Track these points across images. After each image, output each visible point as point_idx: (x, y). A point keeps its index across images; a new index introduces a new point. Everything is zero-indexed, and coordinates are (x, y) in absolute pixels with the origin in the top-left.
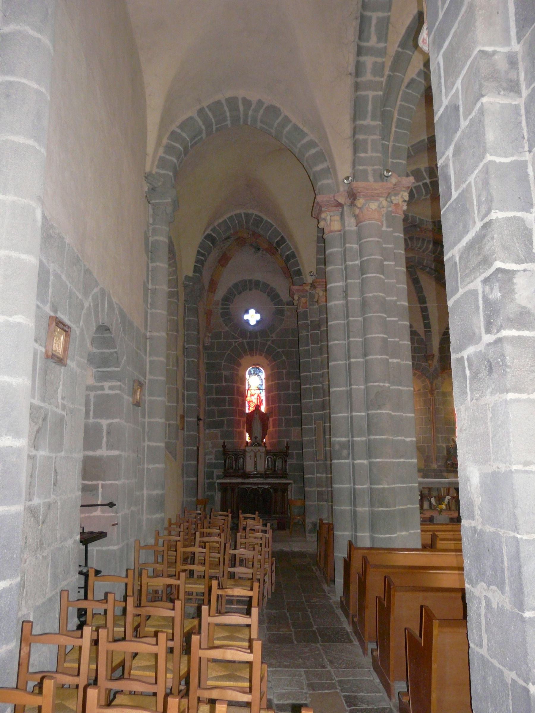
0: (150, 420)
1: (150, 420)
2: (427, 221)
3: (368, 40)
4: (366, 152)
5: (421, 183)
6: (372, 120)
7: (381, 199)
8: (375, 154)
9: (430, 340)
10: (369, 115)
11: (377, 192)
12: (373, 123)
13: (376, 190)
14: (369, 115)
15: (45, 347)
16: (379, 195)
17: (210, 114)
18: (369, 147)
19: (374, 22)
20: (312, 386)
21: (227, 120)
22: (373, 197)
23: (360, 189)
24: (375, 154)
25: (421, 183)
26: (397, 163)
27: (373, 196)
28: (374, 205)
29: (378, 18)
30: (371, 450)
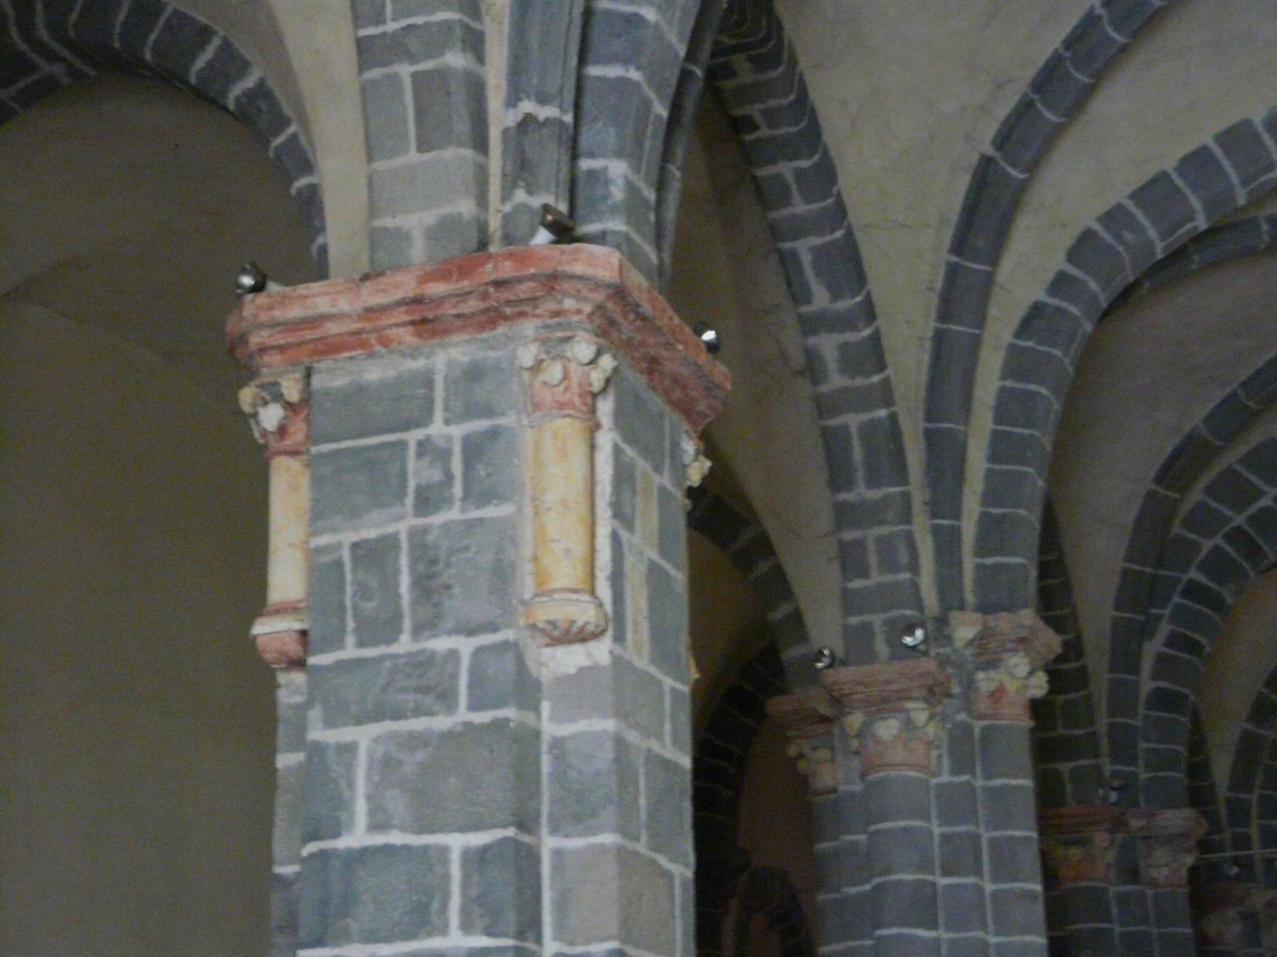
3: (808, 301)
7: (910, 705)
10: (860, 473)
11: (893, 687)
12: (875, 494)
13: (888, 682)
14: (860, 473)
15: (537, 595)
16: (903, 695)
17: (546, 766)
18: (873, 559)
19: (806, 259)
20: (405, 644)
21: (807, 202)
22: (883, 705)
23: (846, 686)
26: (995, 566)
27: (885, 700)
28: (888, 729)
29: (812, 249)
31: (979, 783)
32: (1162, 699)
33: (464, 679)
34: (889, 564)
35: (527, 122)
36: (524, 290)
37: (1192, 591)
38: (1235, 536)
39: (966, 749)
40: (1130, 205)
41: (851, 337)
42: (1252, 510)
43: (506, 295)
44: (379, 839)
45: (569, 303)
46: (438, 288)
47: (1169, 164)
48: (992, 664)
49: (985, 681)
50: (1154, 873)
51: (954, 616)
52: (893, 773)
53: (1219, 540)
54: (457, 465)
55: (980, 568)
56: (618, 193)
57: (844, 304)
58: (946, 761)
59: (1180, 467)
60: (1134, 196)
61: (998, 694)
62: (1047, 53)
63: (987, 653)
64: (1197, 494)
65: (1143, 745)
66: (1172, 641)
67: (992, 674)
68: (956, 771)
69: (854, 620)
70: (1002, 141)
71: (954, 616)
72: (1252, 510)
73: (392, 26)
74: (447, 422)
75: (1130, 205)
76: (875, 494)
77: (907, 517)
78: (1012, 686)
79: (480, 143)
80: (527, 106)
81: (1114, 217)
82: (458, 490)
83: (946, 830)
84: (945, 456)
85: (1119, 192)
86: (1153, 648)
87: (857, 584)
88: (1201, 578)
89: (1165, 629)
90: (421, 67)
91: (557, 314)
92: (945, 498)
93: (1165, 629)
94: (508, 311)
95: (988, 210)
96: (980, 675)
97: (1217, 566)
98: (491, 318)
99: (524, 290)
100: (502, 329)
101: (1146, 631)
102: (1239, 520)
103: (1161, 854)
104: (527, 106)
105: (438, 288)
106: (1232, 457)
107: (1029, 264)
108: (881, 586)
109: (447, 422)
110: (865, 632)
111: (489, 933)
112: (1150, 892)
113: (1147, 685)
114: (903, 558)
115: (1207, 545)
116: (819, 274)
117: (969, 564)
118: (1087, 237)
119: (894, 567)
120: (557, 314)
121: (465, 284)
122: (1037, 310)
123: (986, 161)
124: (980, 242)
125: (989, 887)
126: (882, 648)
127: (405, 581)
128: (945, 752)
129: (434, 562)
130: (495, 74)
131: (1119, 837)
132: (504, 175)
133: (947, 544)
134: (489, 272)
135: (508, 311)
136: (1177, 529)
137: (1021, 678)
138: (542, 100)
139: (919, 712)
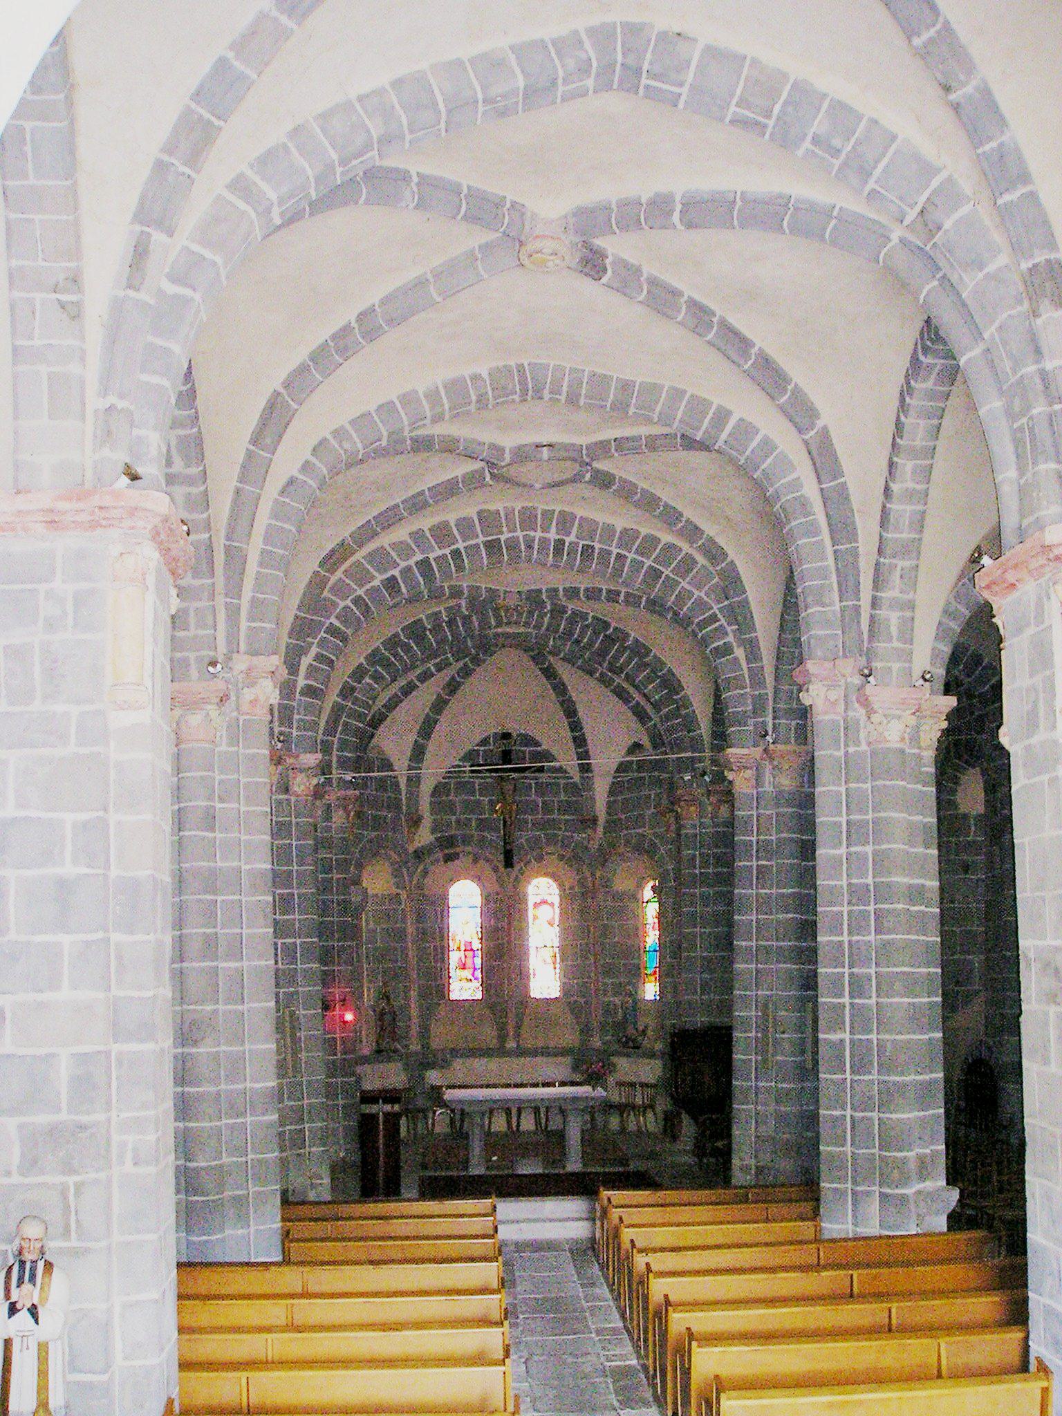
0: (750, 943)
1: (750, 943)
2: (506, 592)
4: (187, 629)
5: (447, 551)
6: (193, 578)
7: (209, 707)
8: (201, 632)
9: (587, 783)
12: (197, 582)
16: (205, 701)
18: (192, 620)
24: (201, 632)
25: (447, 551)
30: (858, 987)
31: (241, 750)
32: (310, 691)
33: (73, 730)
34: (201, 624)
35: (110, 409)
36: (116, 513)
37: (332, 631)
38: (358, 601)
39: (236, 732)
40: (348, 427)
41: (193, 490)
42: (368, 586)
43: (104, 514)
44: (22, 813)
45: (141, 524)
46: (63, 505)
47: (372, 408)
48: (252, 684)
49: (248, 694)
50: (296, 788)
51: (235, 655)
52: (196, 745)
53: (349, 602)
54: (70, 608)
55: (250, 629)
56: (154, 452)
57: (194, 470)
58: (224, 738)
59: (332, 560)
60: (353, 422)
61: (253, 703)
62: (321, 340)
63: (250, 677)
64: (339, 574)
65: (296, 717)
66: (318, 657)
67: (253, 690)
68: (230, 744)
69: (178, 655)
70: (287, 385)
71: (235, 655)
72: (368, 586)
73: (37, 342)
74: (64, 582)
75: (348, 427)
76: (197, 582)
77: (212, 596)
78: (262, 698)
79: (83, 418)
80: (112, 399)
81: (338, 433)
82: (70, 622)
83: (223, 777)
84: (236, 558)
85: (343, 420)
86: (306, 661)
87: (180, 634)
88: (337, 624)
89: (314, 650)
90: (54, 369)
91: (133, 528)
92: (234, 589)
93: (314, 650)
94: (104, 523)
95: (274, 419)
96: (246, 690)
97: (345, 616)
98: (94, 525)
99: (116, 513)
100: (99, 531)
101: (303, 651)
102: (360, 592)
103: (301, 778)
104: (112, 399)
105: (63, 505)
106: (359, 556)
107: (289, 458)
108: (196, 636)
109: (64, 582)
110: (185, 663)
111: (89, 866)
112: (293, 799)
113: (301, 682)
114: (210, 620)
115: (342, 604)
116: (179, 451)
117: (244, 624)
118: (323, 442)
119: (205, 626)
120: (133, 528)
121: (81, 505)
122: (292, 481)
123: (277, 394)
124: (268, 441)
125: (874, 1036)
126: (194, 673)
127: (37, 670)
128: (224, 732)
129: (56, 661)
130: (92, 372)
131: (280, 767)
132: (95, 436)
133: (233, 613)
134: (96, 500)
135: (104, 523)
136: (326, 593)
137: (269, 693)
138: (121, 396)
139: (212, 710)
